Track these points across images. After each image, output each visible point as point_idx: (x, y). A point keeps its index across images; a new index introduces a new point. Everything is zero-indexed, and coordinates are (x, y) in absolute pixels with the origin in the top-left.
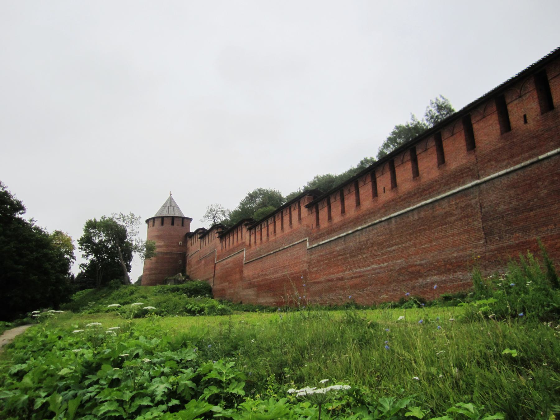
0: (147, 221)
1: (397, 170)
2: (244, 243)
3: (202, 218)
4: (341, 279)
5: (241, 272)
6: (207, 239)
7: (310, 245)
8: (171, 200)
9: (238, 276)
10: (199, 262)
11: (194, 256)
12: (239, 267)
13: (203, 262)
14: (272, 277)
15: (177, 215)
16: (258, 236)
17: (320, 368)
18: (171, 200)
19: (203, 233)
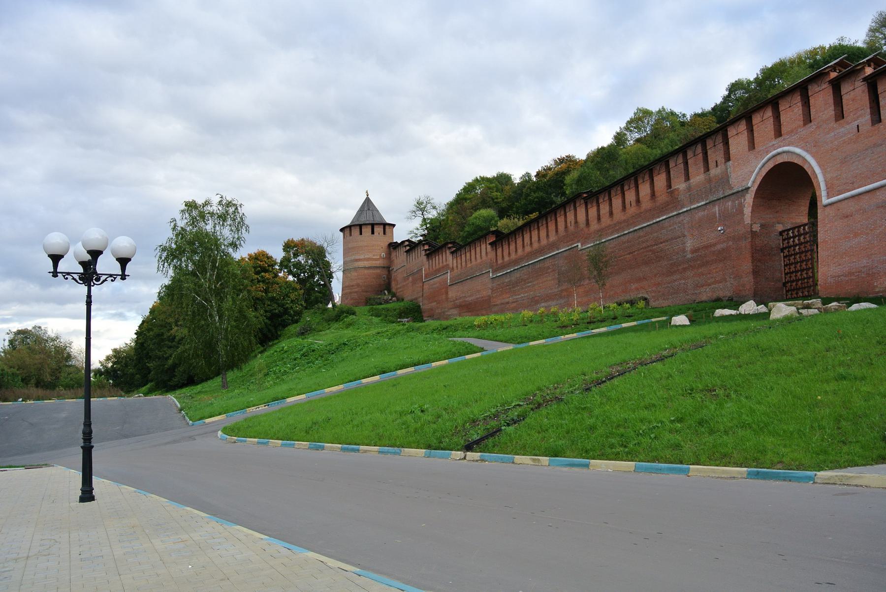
0: (342, 230)
1: (655, 179)
2: (448, 265)
3: (409, 214)
4: (508, 303)
5: (447, 293)
6: (413, 255)
7: (829, 197)
8: (368, 201)
9: (444, 297)
10: (406, 279)
11: (400, 271)
12: (445, 288)
13: (410, 279)
14: (469, 299)
15: (377, 220)
16: (459, 261)
17: (625, 447)
18: (368, 201)
19: (411, 246)
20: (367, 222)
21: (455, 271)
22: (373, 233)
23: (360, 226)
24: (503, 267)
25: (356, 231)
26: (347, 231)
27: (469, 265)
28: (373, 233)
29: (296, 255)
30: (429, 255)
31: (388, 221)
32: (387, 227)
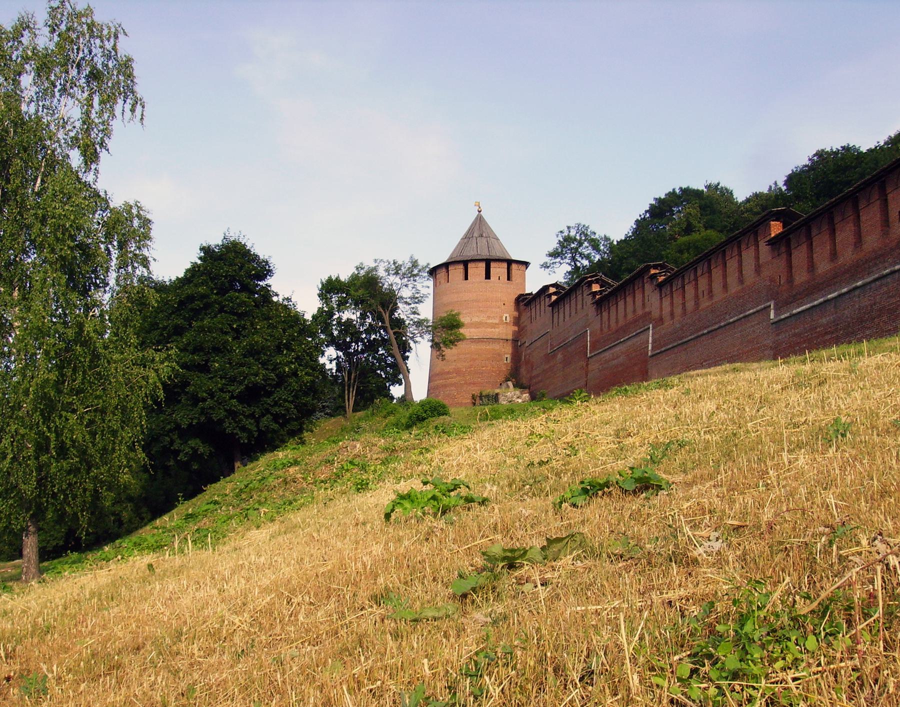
8: (480, 221)
10: (549, 357)
13: (560, 356)
15: (498, 254)
16: (678, 300)
18: (480, 221)
20: (479, 257)
21: (668, 322)
22: (488, 276)
23: (465, 263)
24: (812, 289)
25: (457, 272)
26: (442, 274)
27: (705, 303)
28: (488, 276)
29: (342, 304)
30: (602, 303)
31: (514, 257)
32: (514, 266)
